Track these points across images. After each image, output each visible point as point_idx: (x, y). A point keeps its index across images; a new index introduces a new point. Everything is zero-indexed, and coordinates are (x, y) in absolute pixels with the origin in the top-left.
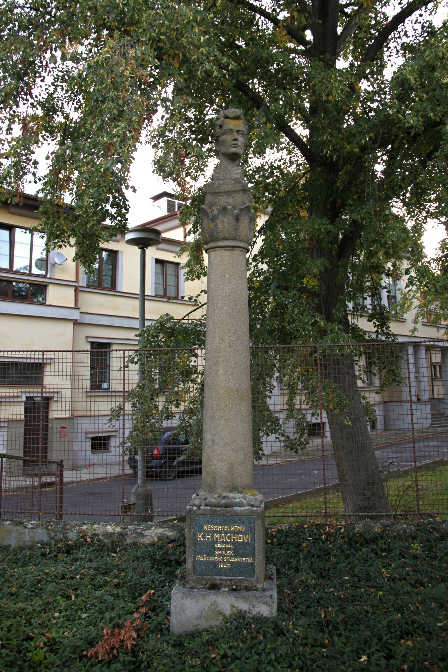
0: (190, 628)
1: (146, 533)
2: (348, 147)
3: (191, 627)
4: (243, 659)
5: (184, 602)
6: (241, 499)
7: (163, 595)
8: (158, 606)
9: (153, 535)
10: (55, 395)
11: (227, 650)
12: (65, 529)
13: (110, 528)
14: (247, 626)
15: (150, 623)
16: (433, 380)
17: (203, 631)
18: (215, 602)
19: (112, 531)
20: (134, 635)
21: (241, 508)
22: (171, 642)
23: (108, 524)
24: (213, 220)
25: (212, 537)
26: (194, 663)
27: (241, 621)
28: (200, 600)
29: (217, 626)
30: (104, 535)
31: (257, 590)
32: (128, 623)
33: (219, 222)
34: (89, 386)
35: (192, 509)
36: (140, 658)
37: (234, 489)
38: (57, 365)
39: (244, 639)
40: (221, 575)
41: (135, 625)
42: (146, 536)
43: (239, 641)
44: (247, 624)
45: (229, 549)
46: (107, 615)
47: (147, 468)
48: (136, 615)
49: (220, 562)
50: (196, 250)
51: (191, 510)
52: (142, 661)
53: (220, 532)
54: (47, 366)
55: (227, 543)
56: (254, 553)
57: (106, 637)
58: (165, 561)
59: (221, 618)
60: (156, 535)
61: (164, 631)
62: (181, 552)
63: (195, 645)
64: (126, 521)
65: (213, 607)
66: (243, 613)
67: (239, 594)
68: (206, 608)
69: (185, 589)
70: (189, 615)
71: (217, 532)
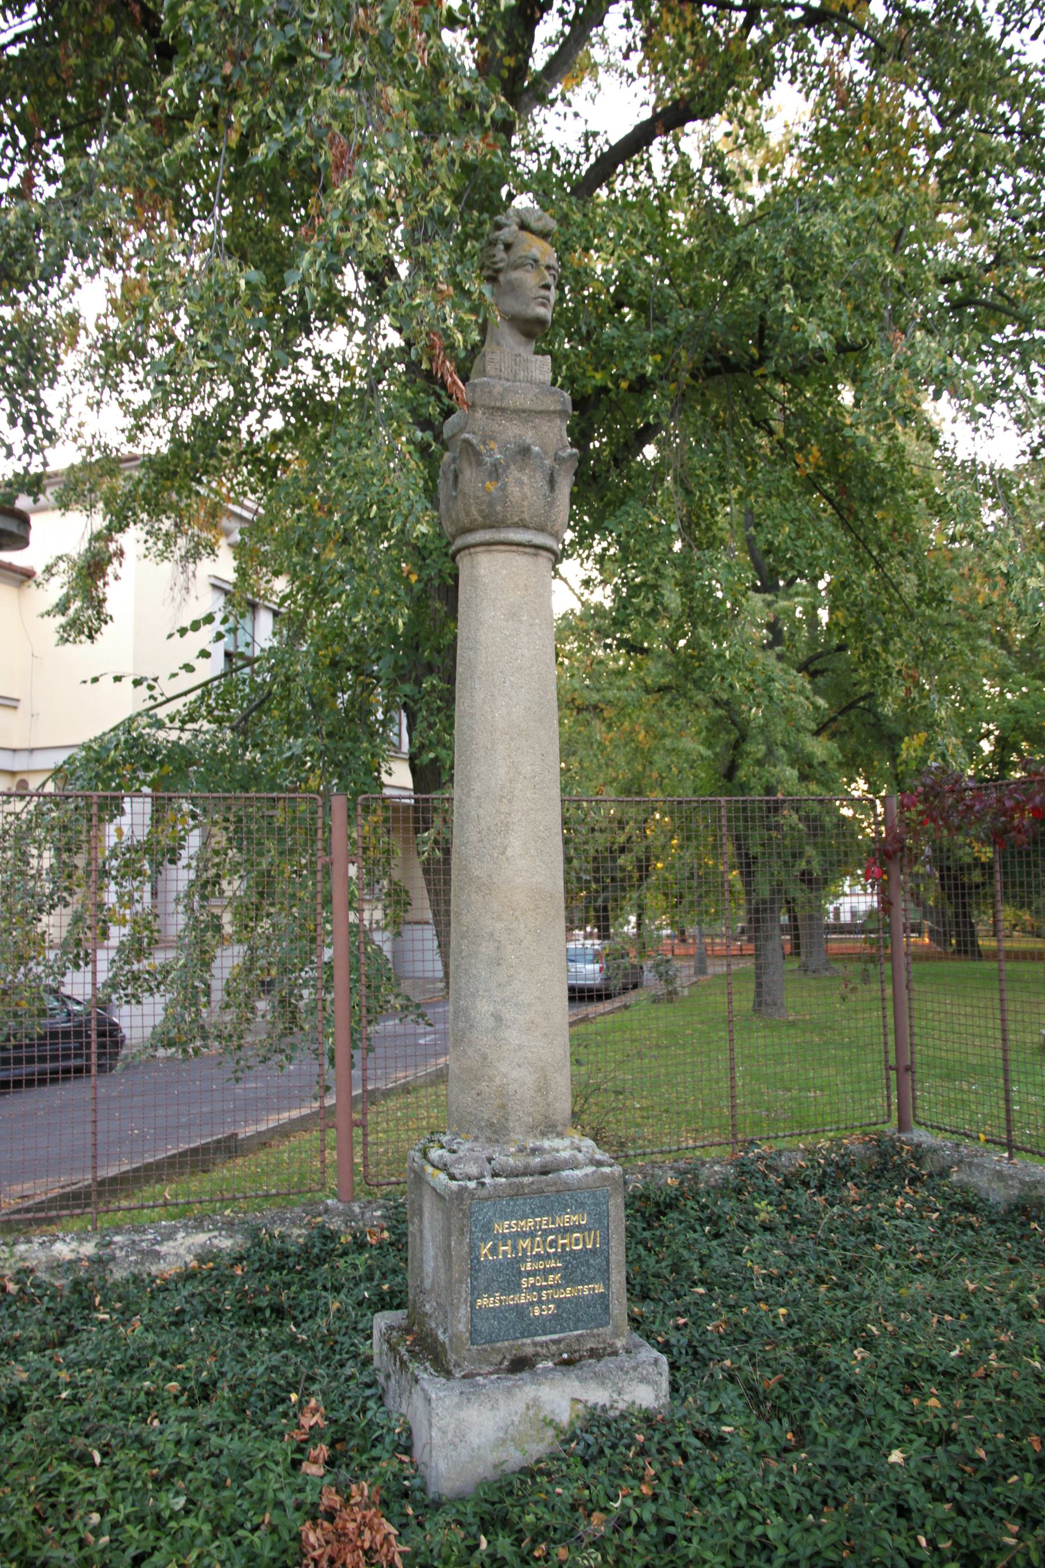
1: (163, 1249)
2: (598, 376)
9: (182, 1251)
13: (63, 1250)
18: (536, 1400)
24: (496, 472)
28: (501, 1402)
31: (615, 1353)
33: (510, 480)
35: (466, 1188)
37: (550, 1129)
40: (536, 1334)
45: (552, 1271)
49: (532, 1304)
53: (532, 1235)
55: (548, 1256)
56: (608, 1270)
59: (550, 1432)
60: (189, 1251)
65: (531, 1412)
68: (516, 1419)
71: (524, 1235)
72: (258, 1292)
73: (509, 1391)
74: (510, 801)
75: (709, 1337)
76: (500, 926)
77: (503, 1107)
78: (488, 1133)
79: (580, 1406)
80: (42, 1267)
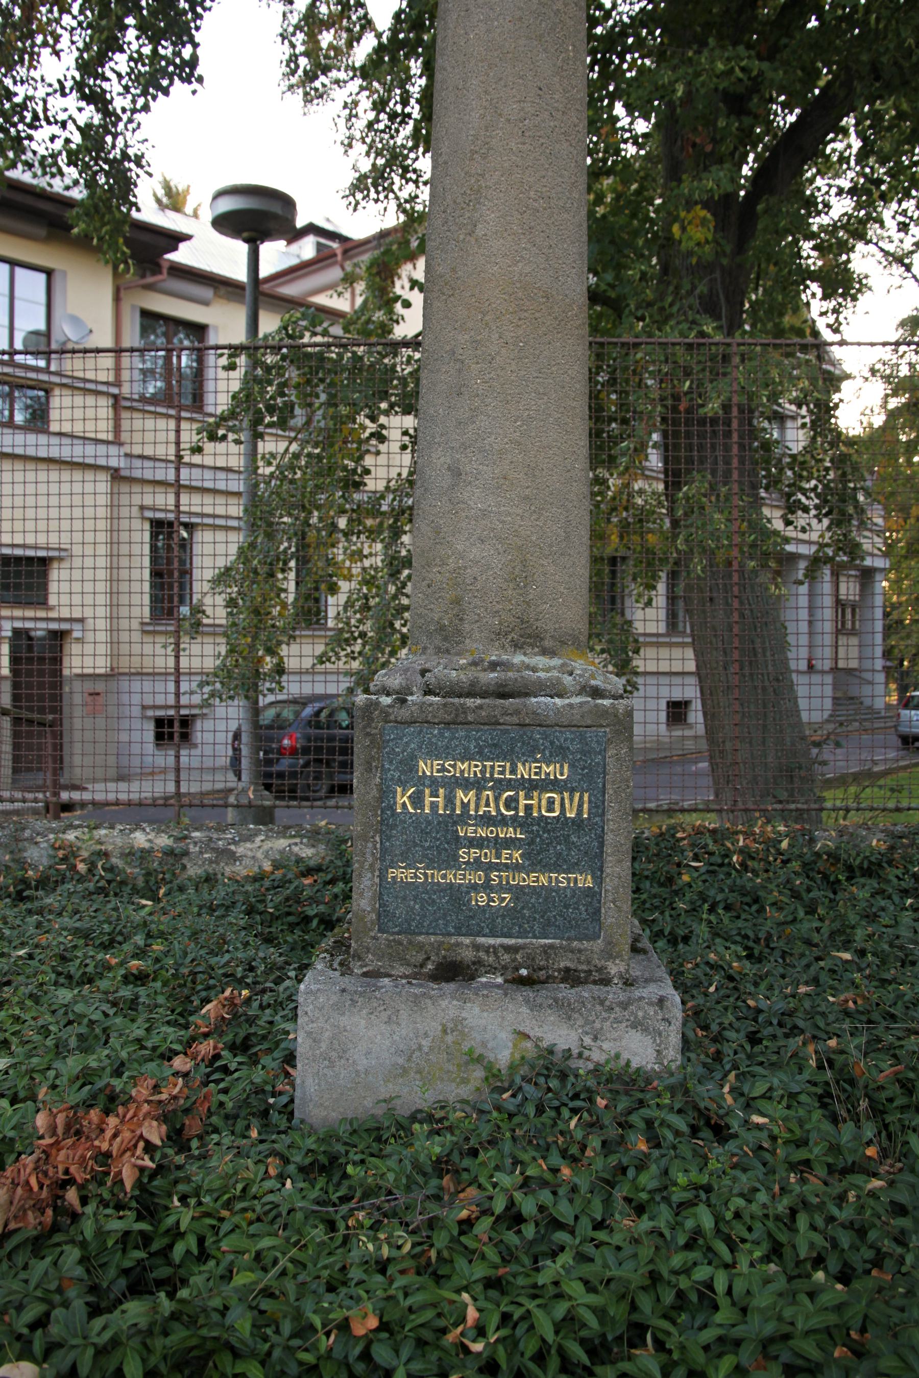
0: (366, 1105)
1: (240, 850)
3: (368, 1103)
4: (585, 1226)
5: (344, 1021)
6: (555, 673)
7: (278, 1005)
8: (258, 1039)
9: (259, 855)
10: (77, 626)
11: (518, 1196)
12: (17, 840)
13: (140, 839)
14: (578, 1103)
15: (225, 1091)
16: (838, 632)
17: (413, 1118)
18: (458, 1022)
19: (147, 845)
20: (154, 1133)
21: (557, 700)
22: (297, 1158)
23: (138, 827)
25: (450, 801)
26: (385, 1252)
27: (554, 1083)
28: (404, 1015)
29: (463, 1101)
30: (123, 855)
31: (606, 981)
32: (141, 1091)
34: (147, 611)
35: (377, 703)
36: (170, 1221)
37: (529, 637)
38: (77, 562)
39: (574, 1150)
40: (479, 934)
41: (164, 1097)
43: (555, 1159)
44: (576, 1096)
45: (509, 843)
46: (72, 1064)
47: (268, 775)
48: (179, 1063)
49: (474, 887)
50: (378, 273)
51: (371, 706)
52: (176, 1234)
53: (478, 785)
54: (55, 565)
55: (503, 821)
57: (48, 1141)
58: (291, 919)
59: (479, 1073)
60: (267, 856)
61: (274, 1116)
62: (336, 896)
63: (387, 1170)
64: (186, 820)
65: (449, 1039)
67: (543, 995)
68: (426, 1043)
69: (347, 979)
71: (466, 784)
72: (313, 900)
74: (484, 157)
76: (463, 338)
77: (457, 601)
78: (438, 641)
79: (529, 1045)
80: (116, 853)
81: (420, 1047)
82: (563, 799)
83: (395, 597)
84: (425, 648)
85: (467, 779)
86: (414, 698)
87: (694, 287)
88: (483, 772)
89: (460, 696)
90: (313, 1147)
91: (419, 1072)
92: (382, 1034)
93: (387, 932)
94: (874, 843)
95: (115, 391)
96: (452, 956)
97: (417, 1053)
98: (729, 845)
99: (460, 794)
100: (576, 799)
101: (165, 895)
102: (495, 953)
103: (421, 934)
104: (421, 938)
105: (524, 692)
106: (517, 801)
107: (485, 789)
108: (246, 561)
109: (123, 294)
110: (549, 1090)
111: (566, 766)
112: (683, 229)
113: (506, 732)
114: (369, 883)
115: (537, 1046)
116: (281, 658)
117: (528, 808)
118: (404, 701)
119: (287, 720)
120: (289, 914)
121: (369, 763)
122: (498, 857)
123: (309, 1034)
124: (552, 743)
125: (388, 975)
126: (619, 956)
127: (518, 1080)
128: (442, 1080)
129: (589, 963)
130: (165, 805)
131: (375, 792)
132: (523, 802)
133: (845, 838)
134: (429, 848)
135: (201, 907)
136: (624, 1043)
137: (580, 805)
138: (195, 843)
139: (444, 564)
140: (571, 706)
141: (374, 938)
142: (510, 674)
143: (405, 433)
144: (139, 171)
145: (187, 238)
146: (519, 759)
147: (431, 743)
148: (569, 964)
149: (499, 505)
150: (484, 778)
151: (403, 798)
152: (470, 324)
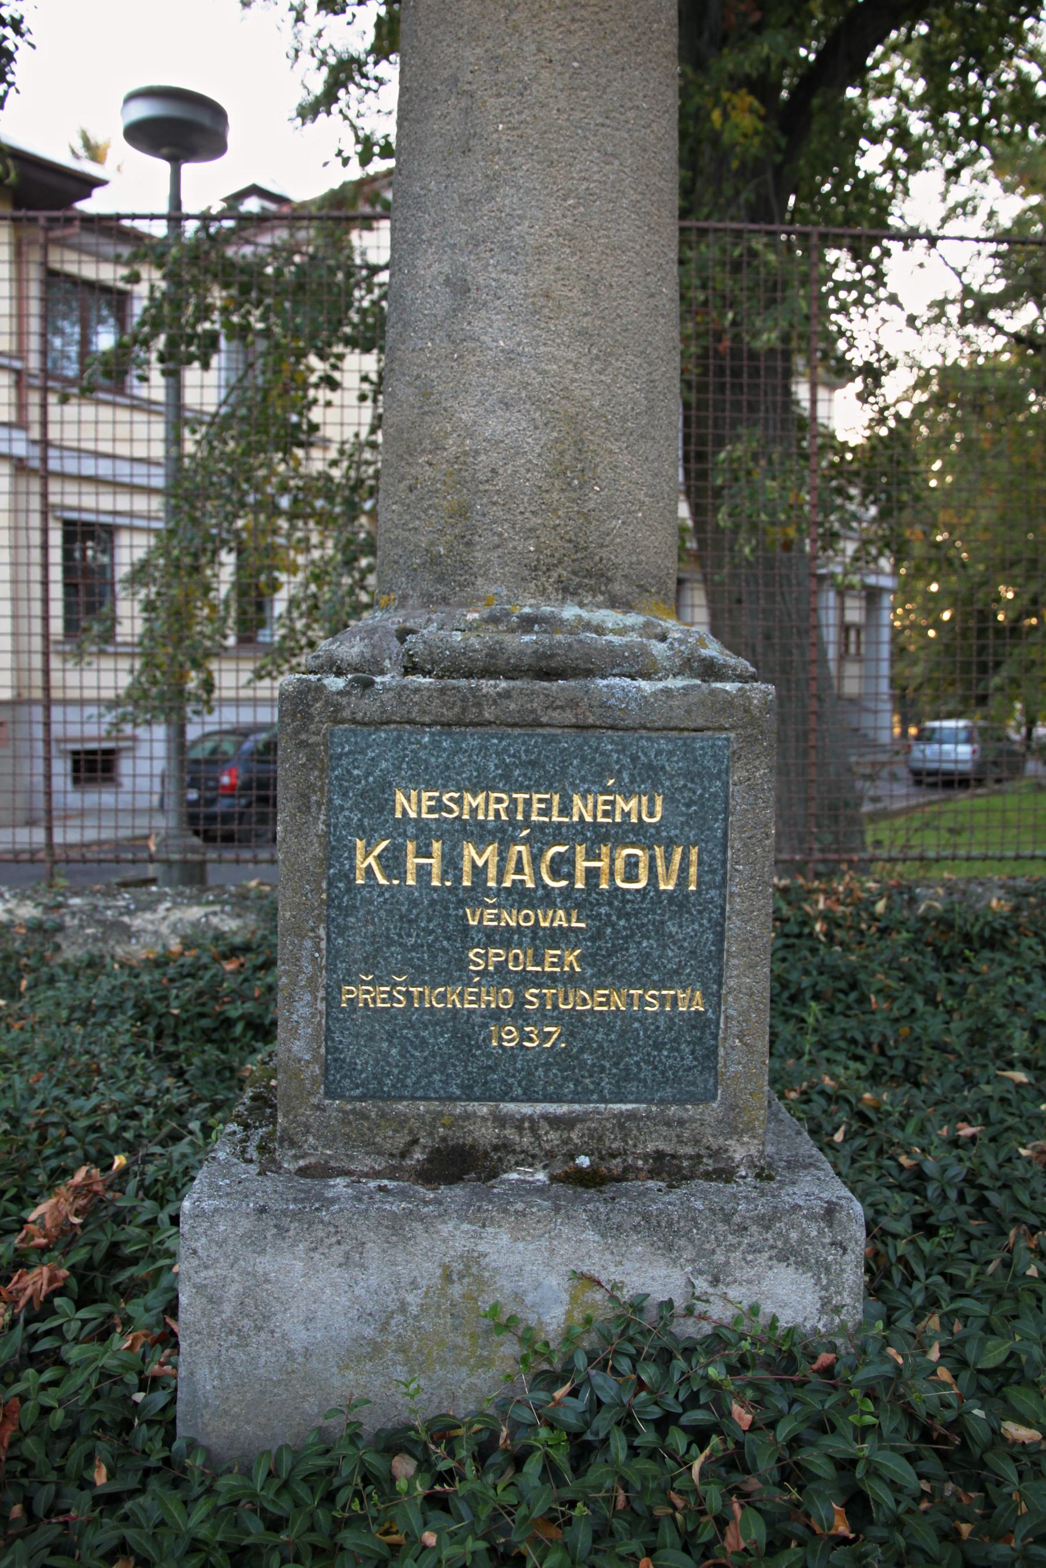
1: (137, 922)
5: (264, 1264)
6: (634, 637)
9: (164, 929)
18: (471, 1260)
21: (646, 686)
25: (452, 863)
27: (649, 1373)
28: (373, 1250)
31: (725, 1174)
35: (320, 688)
37: (589, 576)
40: (505, 1096)
42: (137, 934)
44: (693, 1401)
45: (558, 937)
49: (496, 1015)
53: (501, 834)
55: (546, 899)
58: (205, 1023)
59: (509, 1348)
60: (174, 929)
61: (141, 1432)
64: (62, 882)
65: (456, 1290)
66: (651, 1316)
69: (269, 1183)
70: (299, 1337)
71: (480, 833)
72: (239, 995)
73: (395, 1227)
75: (1020, 1171)
76: (472, 54)
79: (599, 1296)
81: (403, 1308)
82: (652, 859)
83: (351, 592)
84: (404, 597)
85: (482, 825)
86: (387, 678)
87: (737, 193)
88: (511, 811)
89: (469, 675)
90: (203, 1532)
91: (402, 1349)
92: (333, 1285)
93: (341, 1097)
94: (994, 903)
95: (17, 364)
96: (457, 1137)
97: (399, 1318)
98: (807, 908)
99: (469, 851)
100: (677, 857)
101: (29, 988)
102: (533, 1129)
103: (402, 1098)
104: (401, 1106)
105: (585, 669)
106: (572, 863)
107: (515, 841)
108: (166, 553)
109: (24, 249)
110: (641, 1385)
111: (659, 801)
112: (726, 116)
113: (554, 739)
114: (306, 1011)
115: (613, 1298)
116: (210, 673)
117: (592, 874)
118: (368, 684)
119: (225, 753)
120: (202, 1015)
121: (305, 796)
122: (539, 961)
123: (200, 1288)
124: (634, 759)
125: (348, 1173)
126: (749, 1129)
127: (581, 1361)
128: (443, 1362)
129: (697, 1142)
130: (32, 861)
131: (316, 849)
132: (582, 864)
133: (956, 897)
134: (415, 948)
135: (72, 1009)
136: (765, 1285)
137: (684, 869)
138: (73, 914)
139: (439, 448)
140: (667, 692)
141: (318, 1107)
142: (559, 637)
143: (365, 379)
144: (18, 40)
145: (101, 183)
146: (575, 787)
147: (416, 760)
148: (662, 1146)
149: (535, 342)
150: (512, 822)
151: (366, 860)
152: (485, 29)
